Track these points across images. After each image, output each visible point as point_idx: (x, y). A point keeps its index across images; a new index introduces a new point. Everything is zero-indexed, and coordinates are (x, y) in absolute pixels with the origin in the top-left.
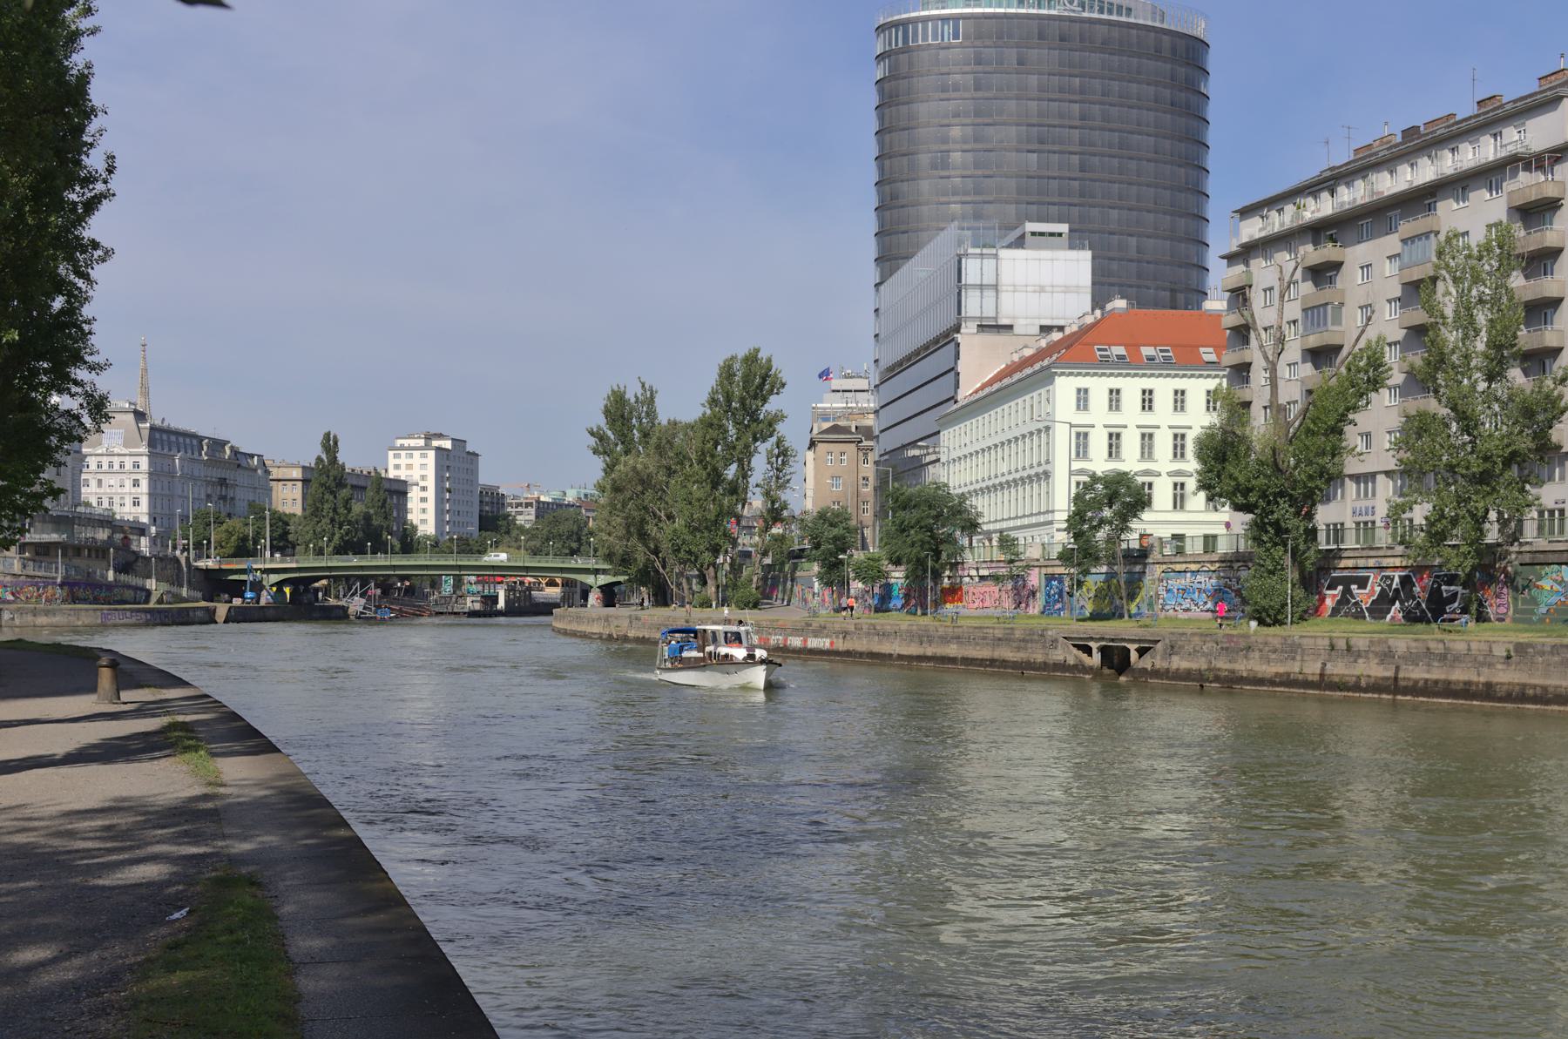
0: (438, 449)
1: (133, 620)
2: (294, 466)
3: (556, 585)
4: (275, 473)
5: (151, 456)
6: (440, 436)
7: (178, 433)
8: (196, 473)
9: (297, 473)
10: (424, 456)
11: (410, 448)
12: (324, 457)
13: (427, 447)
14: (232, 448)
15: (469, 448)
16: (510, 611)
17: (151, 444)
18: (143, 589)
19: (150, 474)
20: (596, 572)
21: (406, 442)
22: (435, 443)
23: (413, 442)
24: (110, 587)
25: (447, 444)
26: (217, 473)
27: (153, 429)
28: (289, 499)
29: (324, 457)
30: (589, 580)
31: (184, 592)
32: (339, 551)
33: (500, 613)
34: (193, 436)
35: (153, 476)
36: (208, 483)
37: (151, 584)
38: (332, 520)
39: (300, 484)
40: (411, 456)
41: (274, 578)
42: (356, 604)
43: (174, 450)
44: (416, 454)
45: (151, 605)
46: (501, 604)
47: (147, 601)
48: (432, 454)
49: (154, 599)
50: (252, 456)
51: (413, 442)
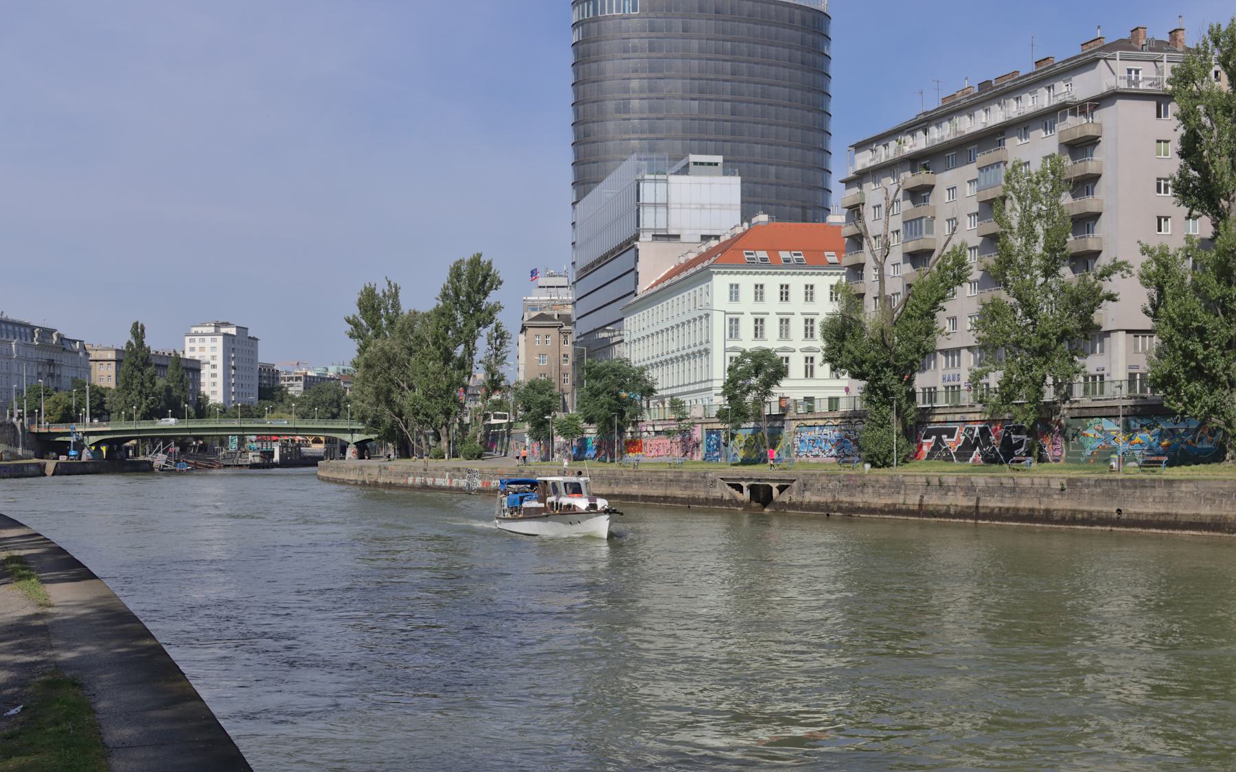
0: (225, 335)
2: (108, 349)
3: (320, 442)
6: (227, 324)
7: (14, 324)
8: (29, 355)
9: (111, 355)
12: (133, 341)
13: (217, 333)
14: (58, 335)
15: (250, 334)
16: (284, 464)
20: (353, 431)
21: (200, 330)
22: (223, 330)
23: (205, 330)
25: (233, 331)
26: (46, 356)
29: (133, 341)
30: (347, 437)
31: (20, 451)
34: (27, 326)
36: (39, 363)
38: (140, 392)
39: (113, 364)
40: (204, 340)
42: (160, 459)
43: (11, 337)
44: (208, 338)
46: (277, 458)
48: (220, 339)
50: (75, 341)
51: (205, 330)
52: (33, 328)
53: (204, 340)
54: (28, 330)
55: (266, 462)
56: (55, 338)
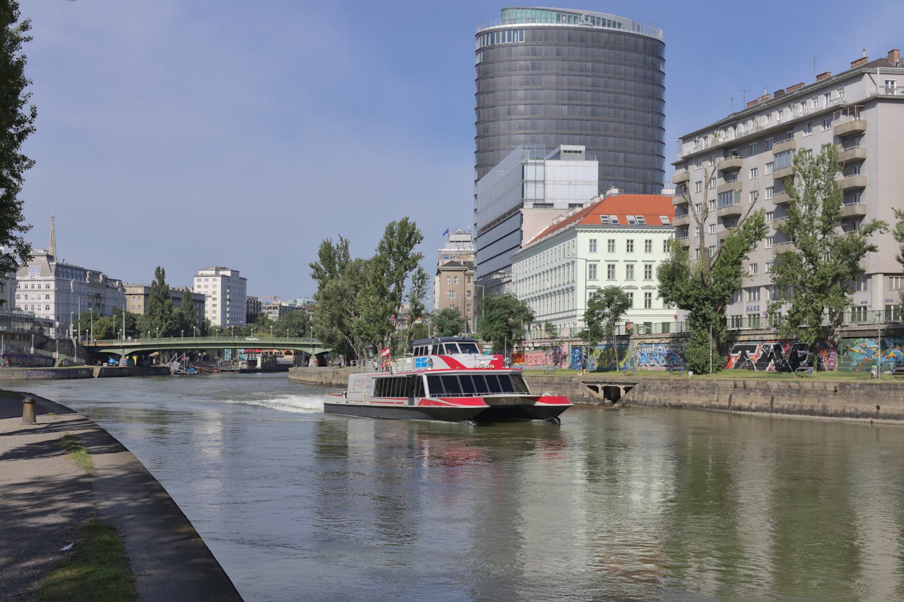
0: (223, 276)
1: (45, 376)
2: (139, 286)
3: (291, 354)
4: (128, 291)
5: (57, 281)
6: (224, 269)
7: (72, 268)
8: (82, 291)
9: (141, 291)
10: (215, 280)
11: (207, 276)
12: (157, 281)
13: (217, 275)
14: (103, 276)
15: (241, 276)
17: (57, 274)
18: (51, 358)
19: (56, 291)
20: (314, 346)
21: (205, 272)
22: (222, 273)
23: (208, 272)
24: (31, 357)
25: (228, 273)
26: (94, 291)
27: (57, 265)
28: (136, 306)
29: (157, 281)
30: (310, 351)
31: (75, 359)
32: (165, 335)
33: (258, 371)
35: (58, 292)
36: (89, 296)
37: (56, 355)
38: (161, 317)
39: (143, 297)
40: (207, 280)
41: (127, 351)
42: (175, 366)
44: (210, 279)
45: (56, 367)
46: (259, 365)
47: (53, 365)
48: (219, 279)
49: (57, 364)
50: (115, 281)
51: (208, 272)
52: (85, 271)
53: (207, 280)
54: (82, 273)
55: (251, 369)
56: (101, 278)
